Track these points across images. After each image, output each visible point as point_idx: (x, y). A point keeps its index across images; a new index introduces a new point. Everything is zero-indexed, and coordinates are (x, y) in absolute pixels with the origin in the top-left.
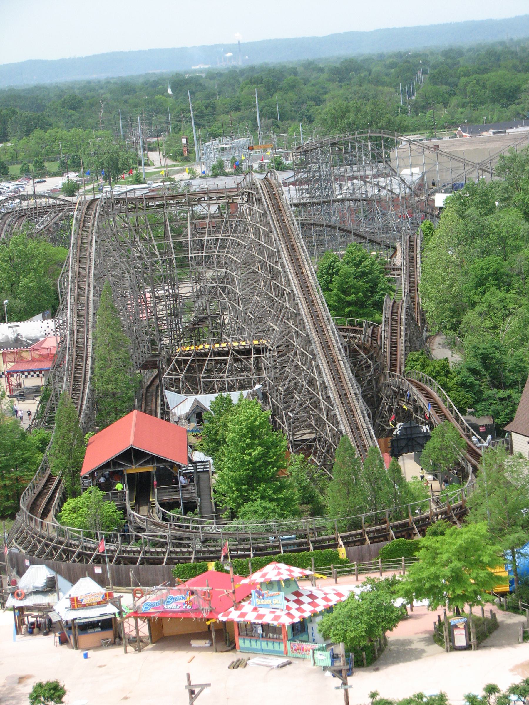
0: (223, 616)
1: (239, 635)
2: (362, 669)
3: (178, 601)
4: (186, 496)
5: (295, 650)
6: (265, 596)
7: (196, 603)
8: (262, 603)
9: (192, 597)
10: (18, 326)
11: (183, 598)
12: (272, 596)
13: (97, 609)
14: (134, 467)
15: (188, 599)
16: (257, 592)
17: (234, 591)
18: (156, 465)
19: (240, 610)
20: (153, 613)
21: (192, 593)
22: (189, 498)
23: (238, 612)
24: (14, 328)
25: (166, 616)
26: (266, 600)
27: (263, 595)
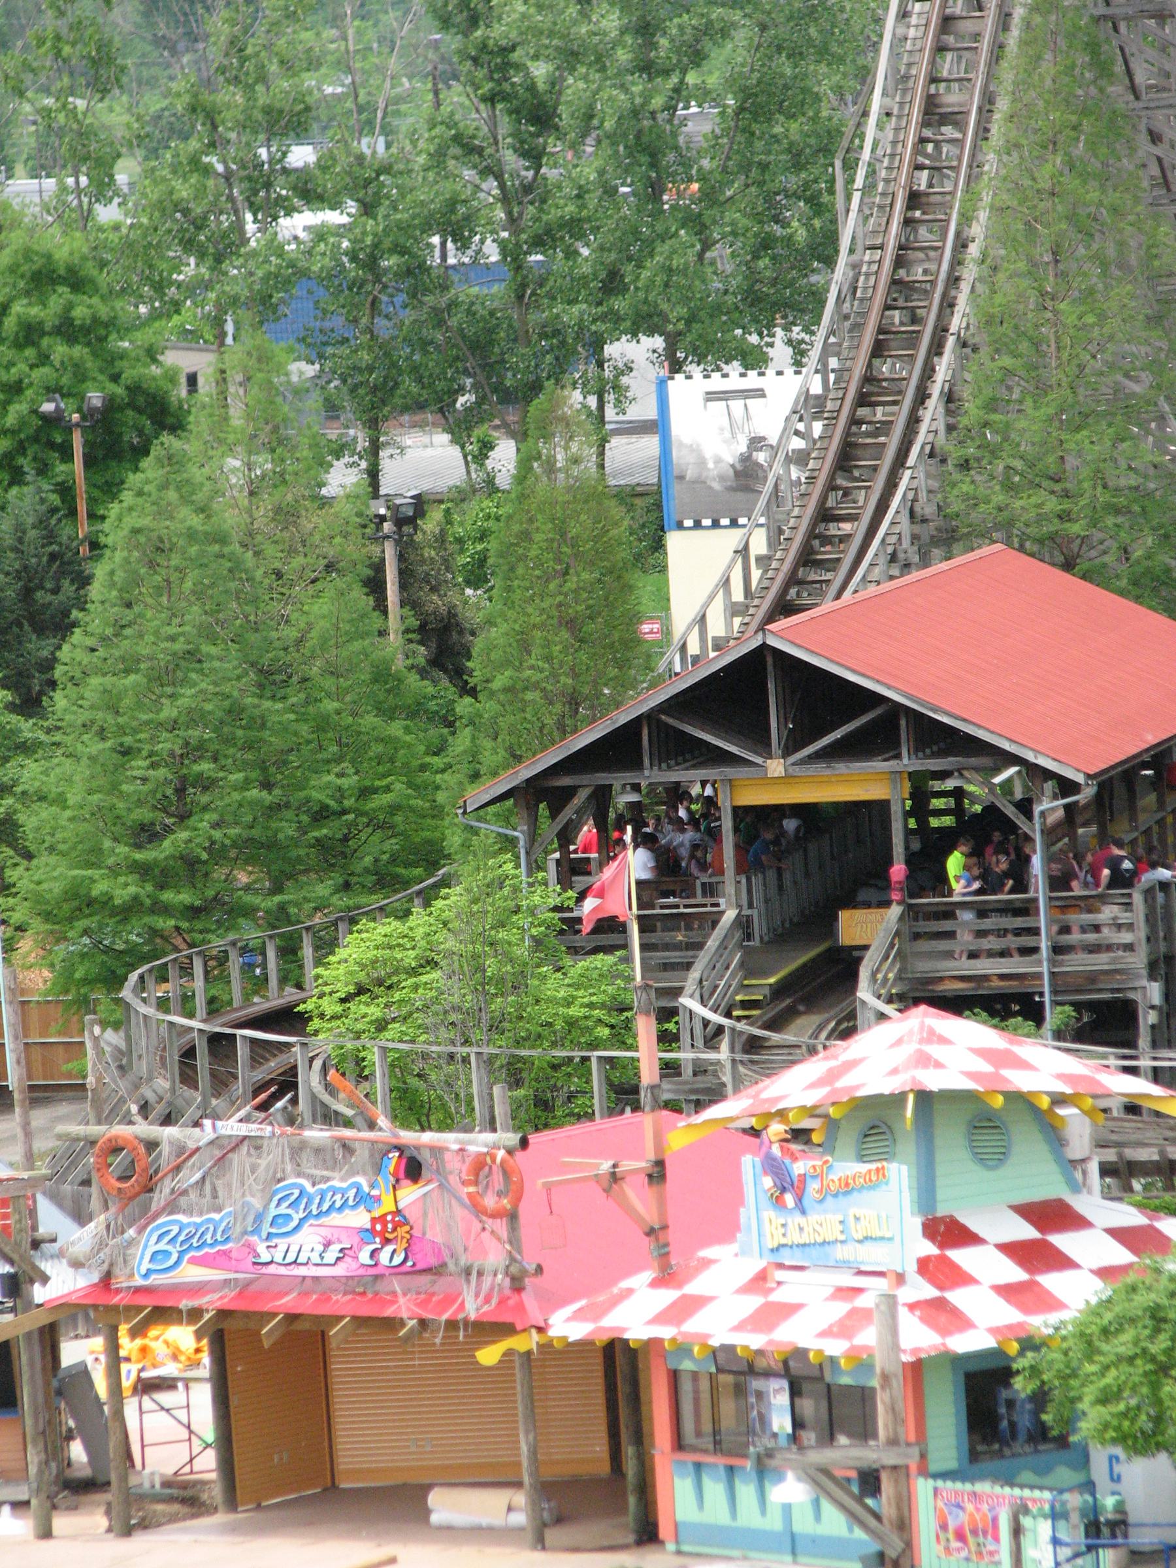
0: (577, 1316)
1: (679, 1445)
2: (915, 1543)
3: (335, 1219)
4: (1077, 963)
5: (960, 1536)
6: (813, 1186)
7: (435, 1234)
8: (794, 1237)
9: (409, 1194)
10: (760, 393)
11: (362, 1199)
12: (847, 1188)
13: (54, 1296)
14: (776, 767)
15: (388, 1205)
16: (772, 1167)
17: (660, 1164)
18: (908, 762)
19: (680, 1286)
20: (198, 1289)
21: (413, 1170)
22: (1092, 978)
23: (667, 1296)
24: (737, 405)
25: (268, 1307)
26: (813, 1218)
27: (798, 1187)
